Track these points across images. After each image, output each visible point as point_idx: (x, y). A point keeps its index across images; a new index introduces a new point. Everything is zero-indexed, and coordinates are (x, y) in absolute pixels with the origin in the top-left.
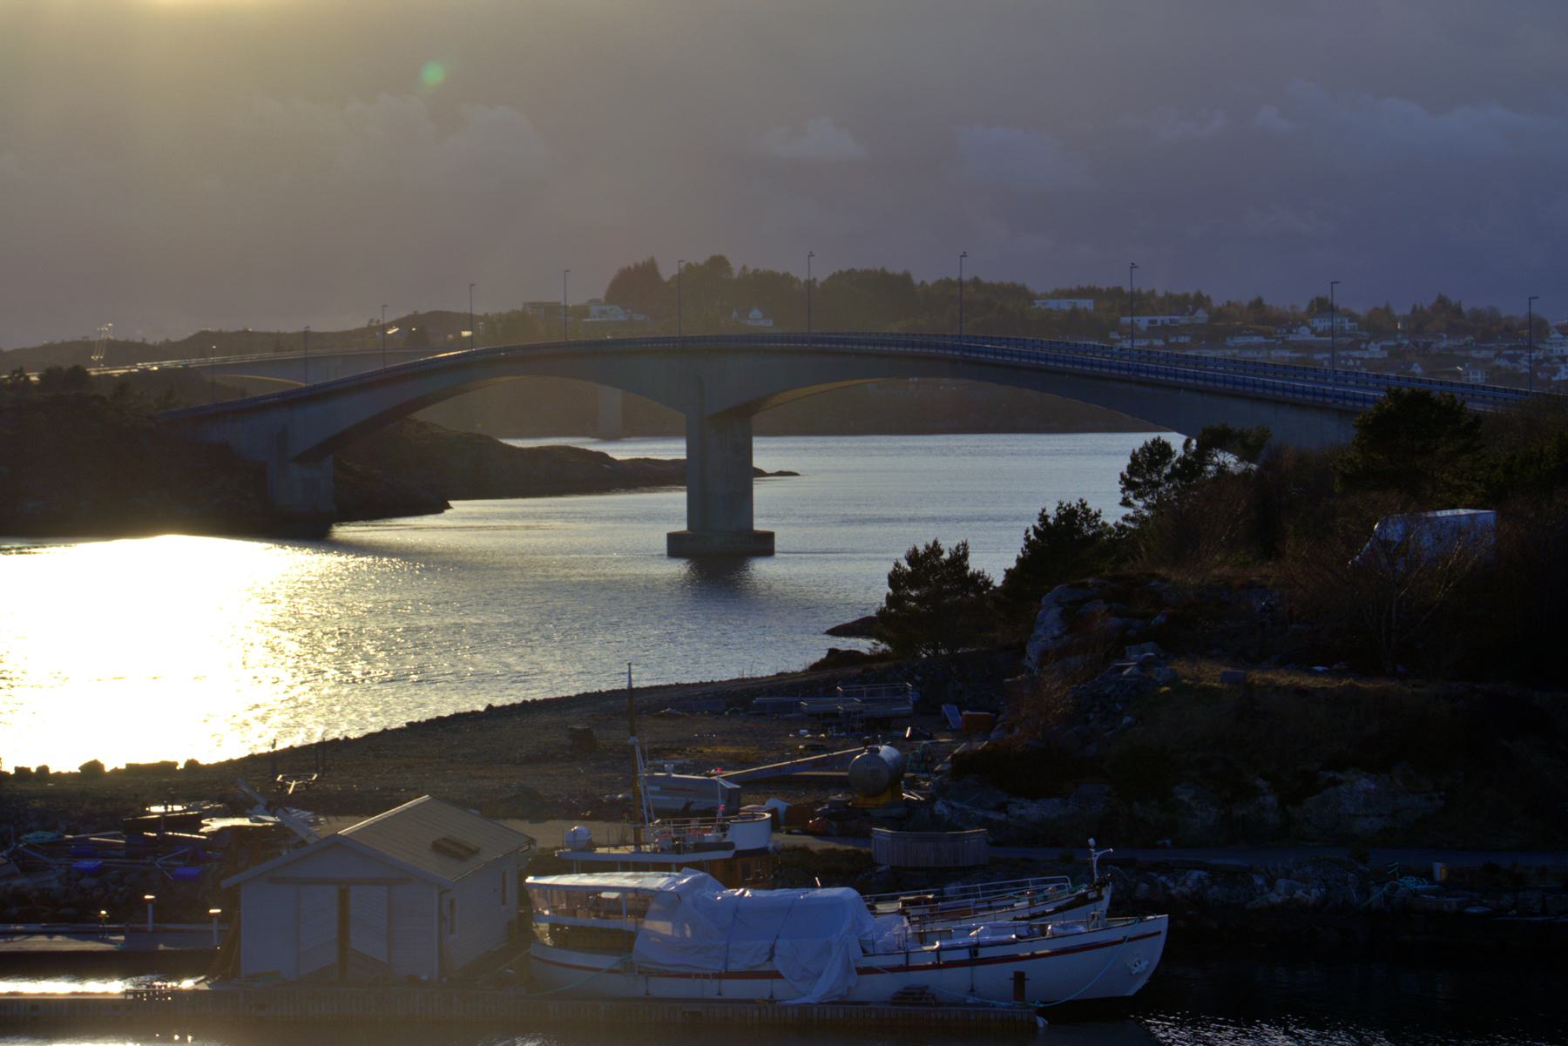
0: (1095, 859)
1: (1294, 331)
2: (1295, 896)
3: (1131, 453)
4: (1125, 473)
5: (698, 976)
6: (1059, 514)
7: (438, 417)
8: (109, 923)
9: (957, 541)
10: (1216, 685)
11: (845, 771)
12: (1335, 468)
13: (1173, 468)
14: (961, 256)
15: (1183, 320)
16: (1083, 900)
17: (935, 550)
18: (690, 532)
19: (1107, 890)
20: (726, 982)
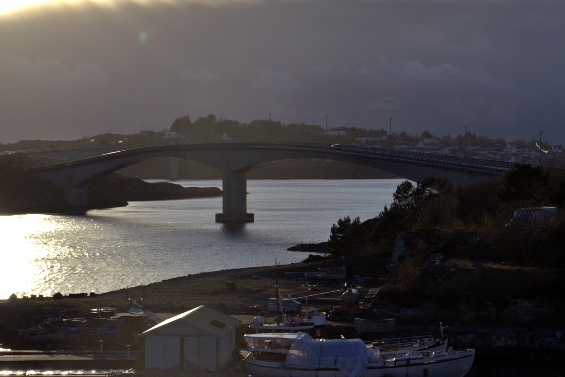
0: (442, 330)
1: (417, 143)
2: (508, 343)
3: (397, 186)
4: (395, 193)
5: (309, 370)
6: (391, 207)
7: (126, 173)
8: (86, 350)
9: (356, 217)
10: (471, 268)
11: (340, 298)
12: (496, 192)
13: (413, 192)
14: (327, 115)
15: (378, 139)
16: (438, 344)
17: (348, 220)
18: (224, 214)
19: (446, 341)
20: (319, 372)
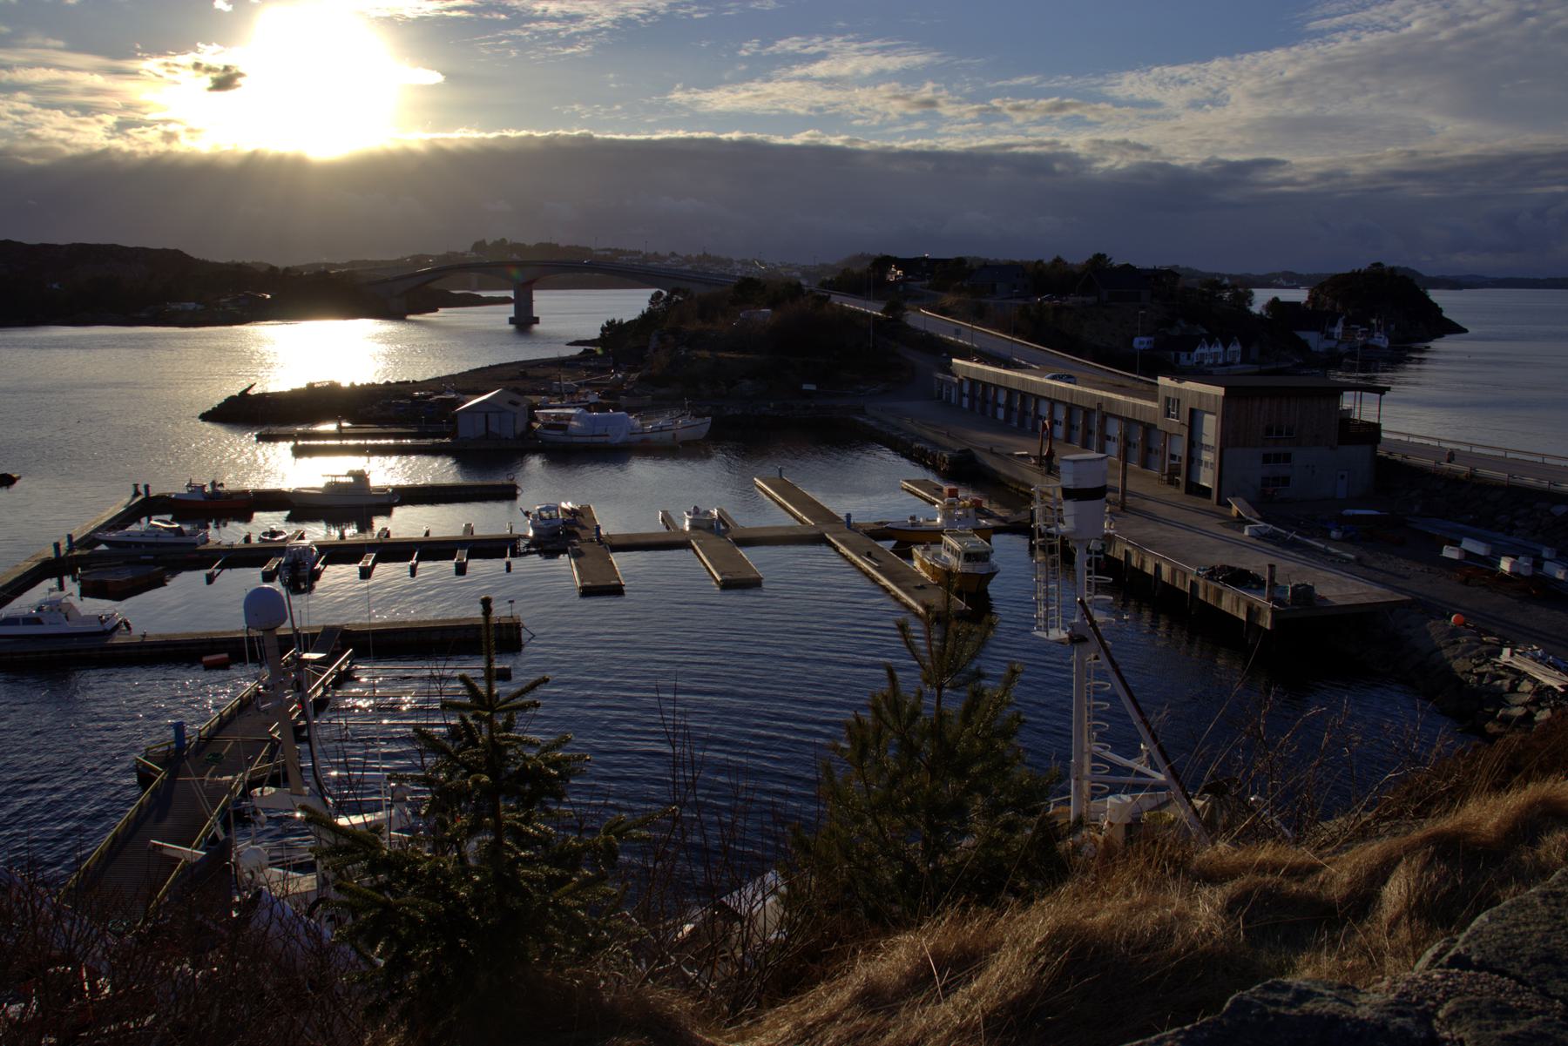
16: (684, 414)
